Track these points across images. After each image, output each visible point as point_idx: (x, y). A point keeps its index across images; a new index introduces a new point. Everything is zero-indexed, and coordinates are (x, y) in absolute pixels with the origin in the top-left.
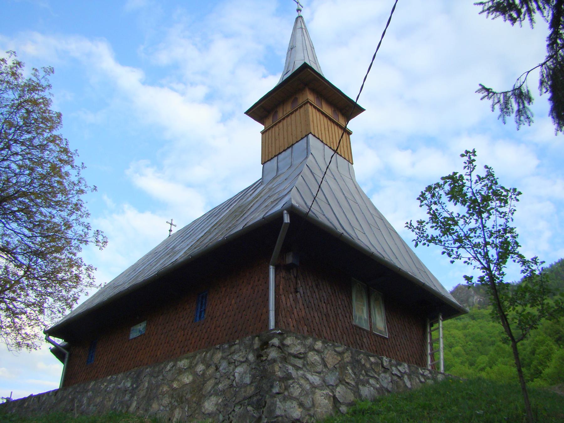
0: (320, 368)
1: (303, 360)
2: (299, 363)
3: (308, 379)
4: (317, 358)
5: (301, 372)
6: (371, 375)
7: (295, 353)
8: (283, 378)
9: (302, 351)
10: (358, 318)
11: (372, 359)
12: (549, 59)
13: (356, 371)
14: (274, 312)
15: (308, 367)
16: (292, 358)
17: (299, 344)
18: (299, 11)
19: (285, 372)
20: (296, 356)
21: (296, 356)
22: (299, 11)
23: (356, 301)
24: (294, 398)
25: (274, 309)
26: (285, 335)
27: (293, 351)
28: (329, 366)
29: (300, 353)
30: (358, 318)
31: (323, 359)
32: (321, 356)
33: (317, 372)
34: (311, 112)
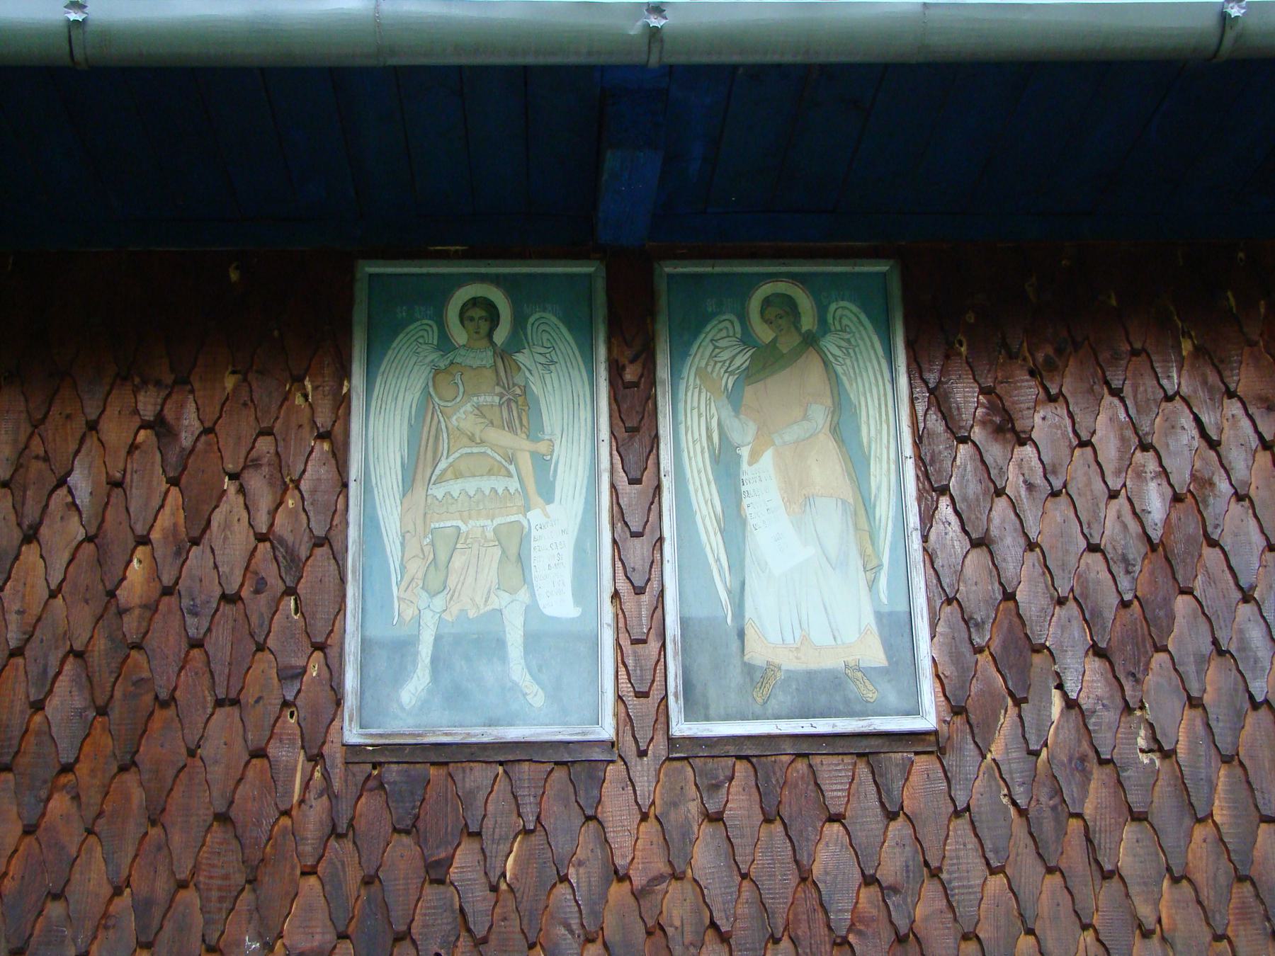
10: (425, 650)
23: (409, 481)
30: (425, 650)
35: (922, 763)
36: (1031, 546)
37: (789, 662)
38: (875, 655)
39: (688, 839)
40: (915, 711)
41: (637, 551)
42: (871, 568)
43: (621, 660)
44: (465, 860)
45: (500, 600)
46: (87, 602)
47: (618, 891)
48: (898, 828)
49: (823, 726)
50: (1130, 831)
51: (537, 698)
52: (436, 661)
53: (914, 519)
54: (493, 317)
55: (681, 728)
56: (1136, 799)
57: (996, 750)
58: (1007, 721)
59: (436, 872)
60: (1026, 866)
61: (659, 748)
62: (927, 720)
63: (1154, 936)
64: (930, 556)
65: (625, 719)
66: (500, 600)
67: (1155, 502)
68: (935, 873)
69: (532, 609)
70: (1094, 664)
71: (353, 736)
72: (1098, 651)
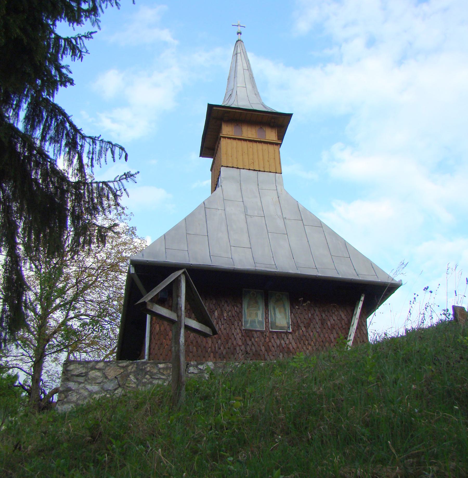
0: (162, 371)
1: (85, 377)
2: (81, 379)
3: (87, 389)
4: (98, 374)
5: (82, 385)
6: (156, 377)
7: (77, 374)
8: (63, 391)
9: (84, 371)
10: (249, 322)
11: (161, 366)
12: (75, 161)
13: (139, 377)
14: (149, 338)
15: (89, 381)
16: (75, 377)
17: (81, 368)
18: (239, 34)
19: (65, 387)
20: (78, 376)
21: (78, 376)
22: (239, 34)
23: (247, 308)
24: (72, 402)
25: (149, 336)
26: (69, 364)
27: (76, 373)
28: (109, 377)
29: (82, 373)
30: (249, 322)
31: (104, 374)
32: (103, 372)
33: (97, 383)
34: (245, 136)
35: (290, 335)
36: (299, 318)
37: (280, 326)
38: (286, 326)
39: (271, 339)
40: (290, 330)
41: (267, 315)
42: (286, 318)
43: (265, 324)
44: (253, 340)
45: (255, 318)
46: (339, 384)
47: (265, 342)
48: (288, 340)
49: (282, 331)
50: (307, 341)
51: (259, 327)
52: (250, 323)
53: (290, 315)
54: (254, 295)
55: (270, 330)
56: (307, 339)
57: (296, 334)
58: (297, 331)
59: (250, 340)
60: (298, 344)
61: (268, 331)
62: (291, 331)
63: (8, 360)
64: (291, 318)
65: (266, 329)
66: (255, 318)
67: (310, 315)
68: (291, 343)
69: (258, 319)
70: (304, 328)
71: (244, 328)
72: (305, 327)
